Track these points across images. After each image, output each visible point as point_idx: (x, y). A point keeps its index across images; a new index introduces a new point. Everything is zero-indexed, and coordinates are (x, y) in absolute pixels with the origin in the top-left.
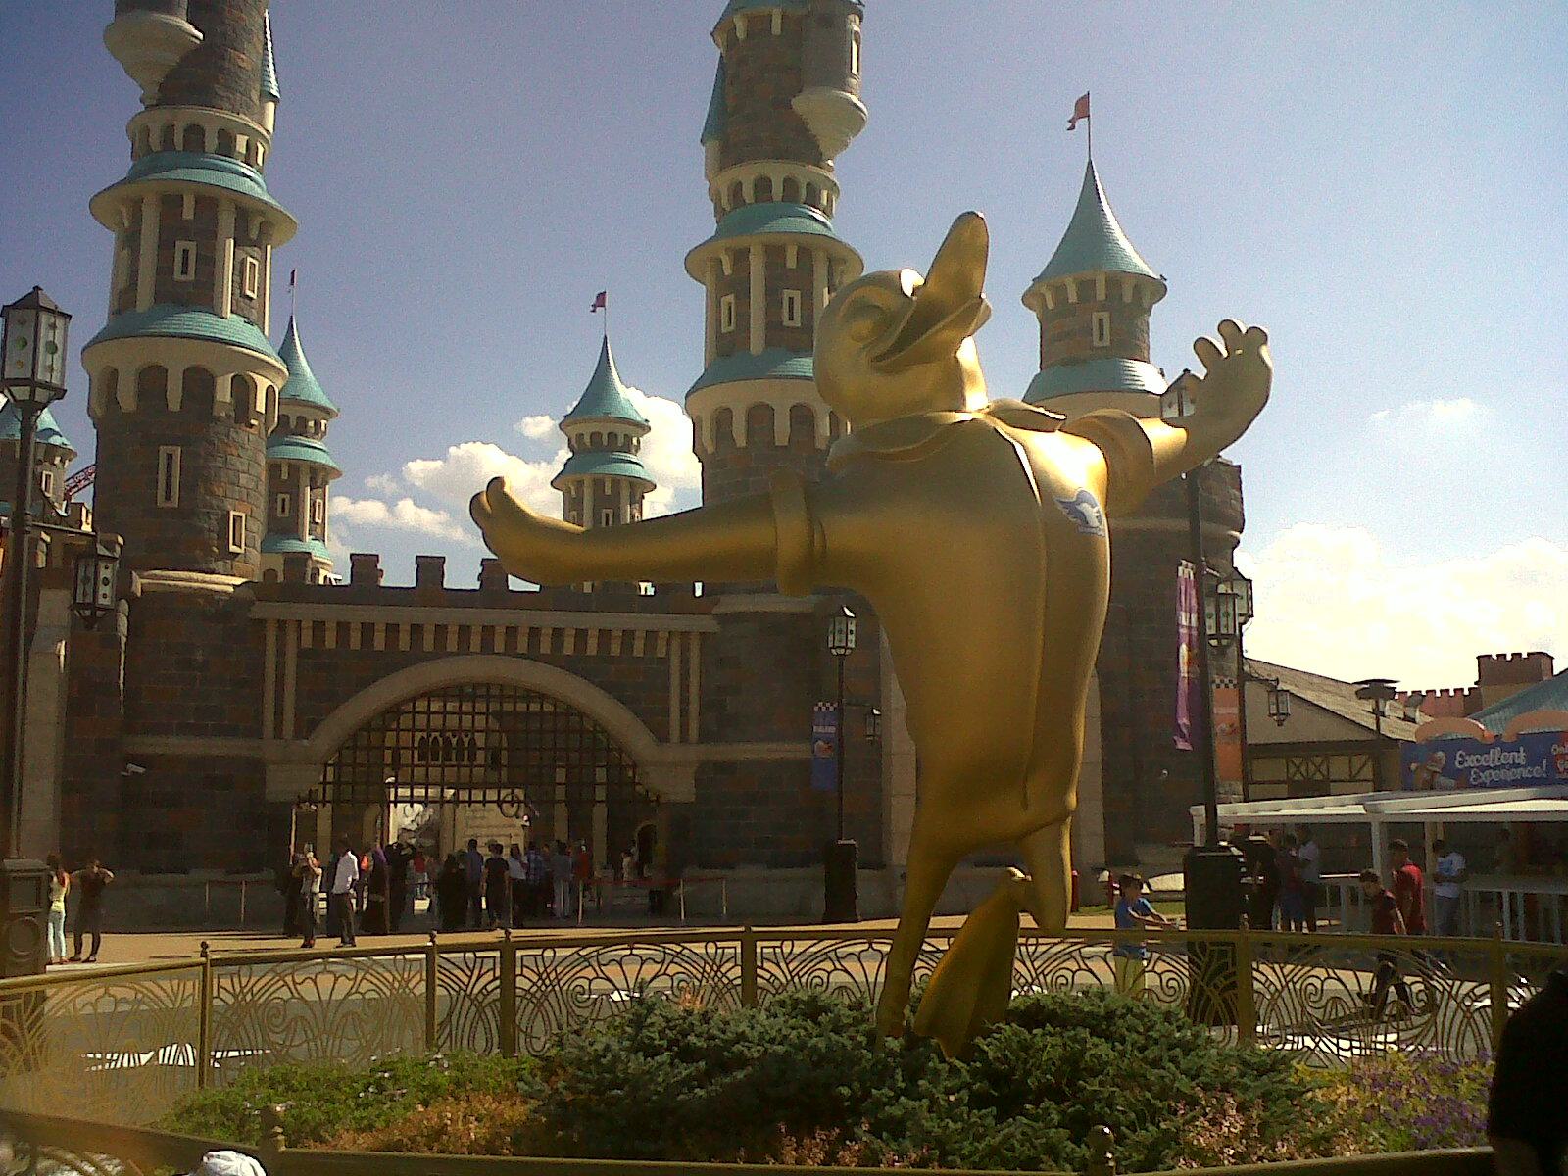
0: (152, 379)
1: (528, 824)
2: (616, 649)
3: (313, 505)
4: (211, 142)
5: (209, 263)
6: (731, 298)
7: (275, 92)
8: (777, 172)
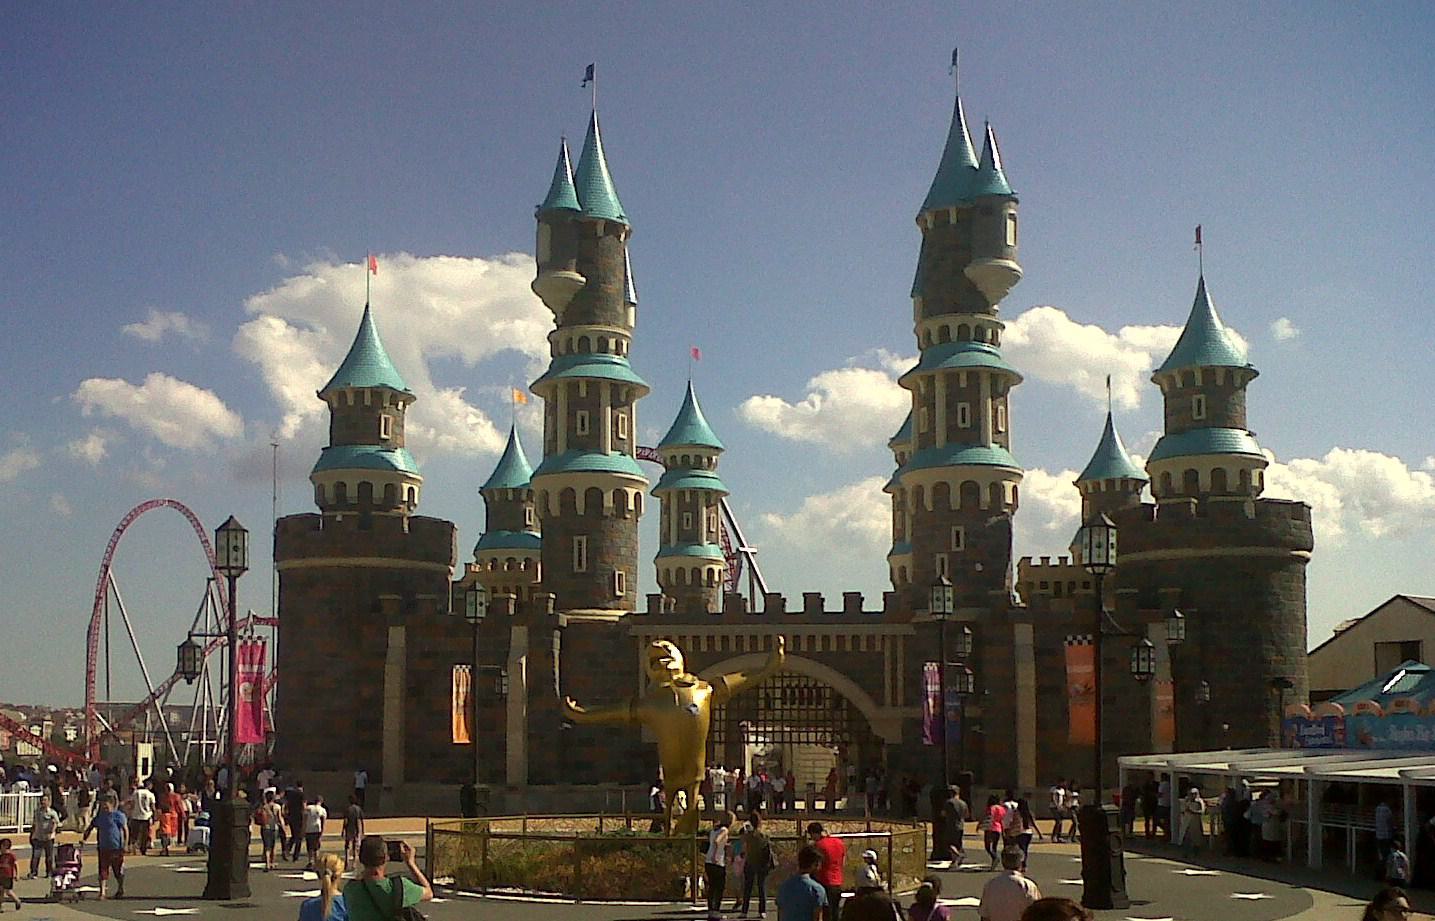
0: (568, 495)
1: (838, 752)
2: (848, 647)
3: (709, 519)
4: (594, 346)
5: (597, 422)
6: (924, 409)
7: (633, 300)
8: (953, 322)
